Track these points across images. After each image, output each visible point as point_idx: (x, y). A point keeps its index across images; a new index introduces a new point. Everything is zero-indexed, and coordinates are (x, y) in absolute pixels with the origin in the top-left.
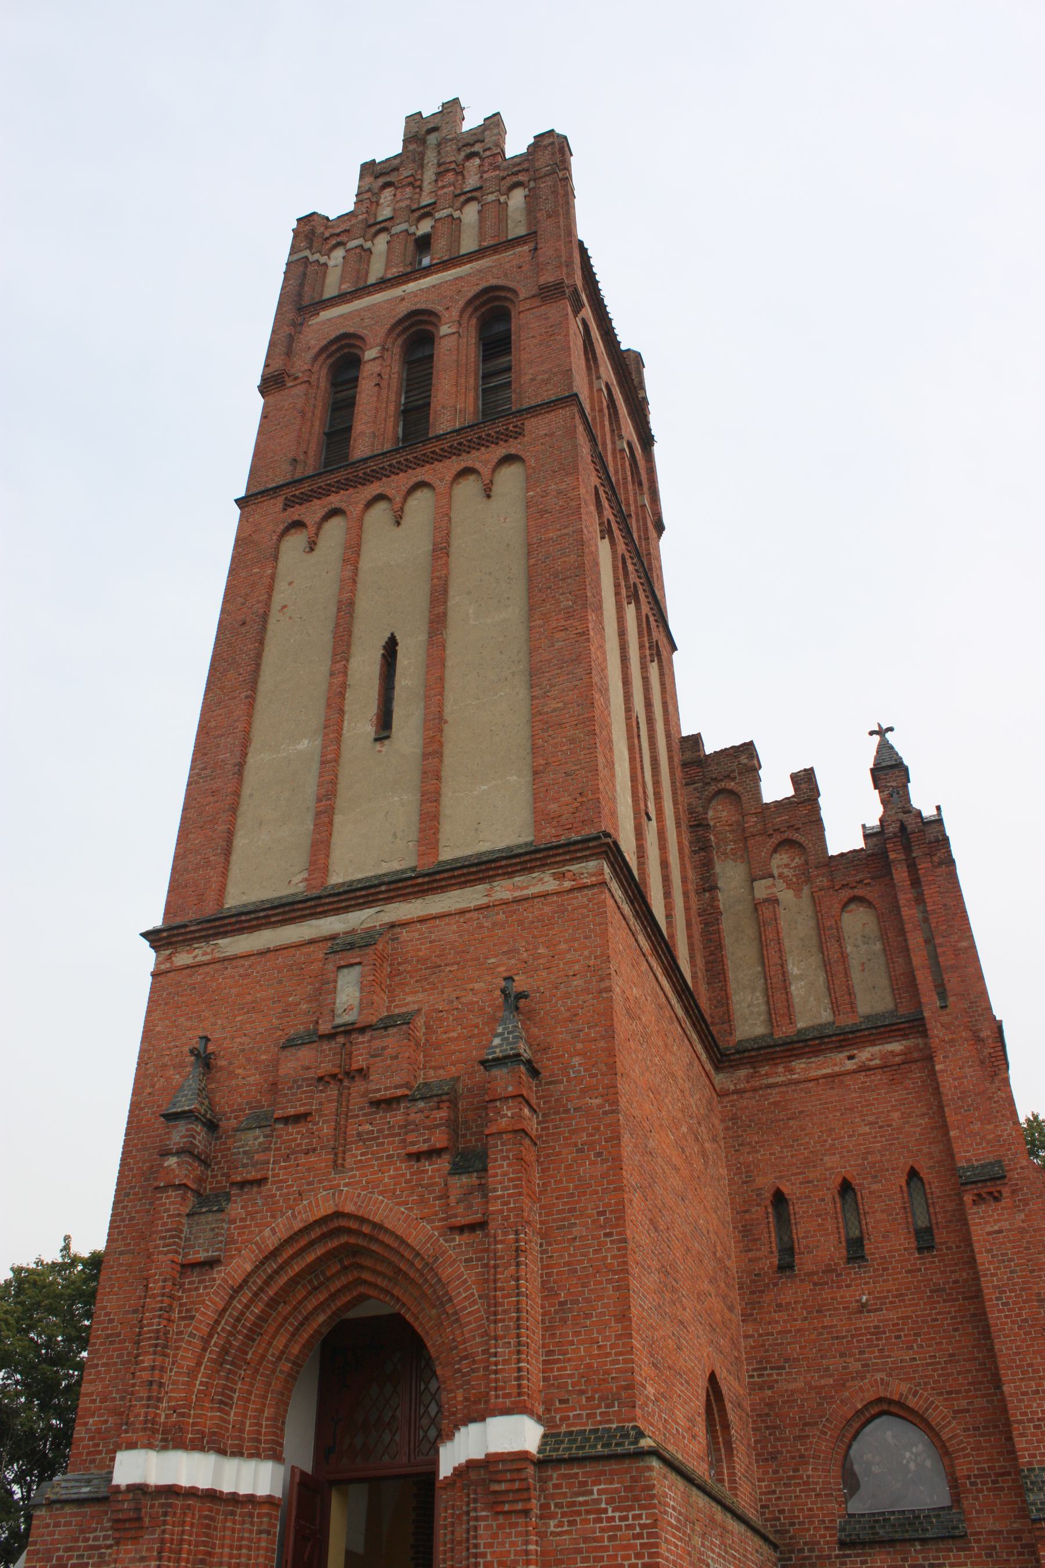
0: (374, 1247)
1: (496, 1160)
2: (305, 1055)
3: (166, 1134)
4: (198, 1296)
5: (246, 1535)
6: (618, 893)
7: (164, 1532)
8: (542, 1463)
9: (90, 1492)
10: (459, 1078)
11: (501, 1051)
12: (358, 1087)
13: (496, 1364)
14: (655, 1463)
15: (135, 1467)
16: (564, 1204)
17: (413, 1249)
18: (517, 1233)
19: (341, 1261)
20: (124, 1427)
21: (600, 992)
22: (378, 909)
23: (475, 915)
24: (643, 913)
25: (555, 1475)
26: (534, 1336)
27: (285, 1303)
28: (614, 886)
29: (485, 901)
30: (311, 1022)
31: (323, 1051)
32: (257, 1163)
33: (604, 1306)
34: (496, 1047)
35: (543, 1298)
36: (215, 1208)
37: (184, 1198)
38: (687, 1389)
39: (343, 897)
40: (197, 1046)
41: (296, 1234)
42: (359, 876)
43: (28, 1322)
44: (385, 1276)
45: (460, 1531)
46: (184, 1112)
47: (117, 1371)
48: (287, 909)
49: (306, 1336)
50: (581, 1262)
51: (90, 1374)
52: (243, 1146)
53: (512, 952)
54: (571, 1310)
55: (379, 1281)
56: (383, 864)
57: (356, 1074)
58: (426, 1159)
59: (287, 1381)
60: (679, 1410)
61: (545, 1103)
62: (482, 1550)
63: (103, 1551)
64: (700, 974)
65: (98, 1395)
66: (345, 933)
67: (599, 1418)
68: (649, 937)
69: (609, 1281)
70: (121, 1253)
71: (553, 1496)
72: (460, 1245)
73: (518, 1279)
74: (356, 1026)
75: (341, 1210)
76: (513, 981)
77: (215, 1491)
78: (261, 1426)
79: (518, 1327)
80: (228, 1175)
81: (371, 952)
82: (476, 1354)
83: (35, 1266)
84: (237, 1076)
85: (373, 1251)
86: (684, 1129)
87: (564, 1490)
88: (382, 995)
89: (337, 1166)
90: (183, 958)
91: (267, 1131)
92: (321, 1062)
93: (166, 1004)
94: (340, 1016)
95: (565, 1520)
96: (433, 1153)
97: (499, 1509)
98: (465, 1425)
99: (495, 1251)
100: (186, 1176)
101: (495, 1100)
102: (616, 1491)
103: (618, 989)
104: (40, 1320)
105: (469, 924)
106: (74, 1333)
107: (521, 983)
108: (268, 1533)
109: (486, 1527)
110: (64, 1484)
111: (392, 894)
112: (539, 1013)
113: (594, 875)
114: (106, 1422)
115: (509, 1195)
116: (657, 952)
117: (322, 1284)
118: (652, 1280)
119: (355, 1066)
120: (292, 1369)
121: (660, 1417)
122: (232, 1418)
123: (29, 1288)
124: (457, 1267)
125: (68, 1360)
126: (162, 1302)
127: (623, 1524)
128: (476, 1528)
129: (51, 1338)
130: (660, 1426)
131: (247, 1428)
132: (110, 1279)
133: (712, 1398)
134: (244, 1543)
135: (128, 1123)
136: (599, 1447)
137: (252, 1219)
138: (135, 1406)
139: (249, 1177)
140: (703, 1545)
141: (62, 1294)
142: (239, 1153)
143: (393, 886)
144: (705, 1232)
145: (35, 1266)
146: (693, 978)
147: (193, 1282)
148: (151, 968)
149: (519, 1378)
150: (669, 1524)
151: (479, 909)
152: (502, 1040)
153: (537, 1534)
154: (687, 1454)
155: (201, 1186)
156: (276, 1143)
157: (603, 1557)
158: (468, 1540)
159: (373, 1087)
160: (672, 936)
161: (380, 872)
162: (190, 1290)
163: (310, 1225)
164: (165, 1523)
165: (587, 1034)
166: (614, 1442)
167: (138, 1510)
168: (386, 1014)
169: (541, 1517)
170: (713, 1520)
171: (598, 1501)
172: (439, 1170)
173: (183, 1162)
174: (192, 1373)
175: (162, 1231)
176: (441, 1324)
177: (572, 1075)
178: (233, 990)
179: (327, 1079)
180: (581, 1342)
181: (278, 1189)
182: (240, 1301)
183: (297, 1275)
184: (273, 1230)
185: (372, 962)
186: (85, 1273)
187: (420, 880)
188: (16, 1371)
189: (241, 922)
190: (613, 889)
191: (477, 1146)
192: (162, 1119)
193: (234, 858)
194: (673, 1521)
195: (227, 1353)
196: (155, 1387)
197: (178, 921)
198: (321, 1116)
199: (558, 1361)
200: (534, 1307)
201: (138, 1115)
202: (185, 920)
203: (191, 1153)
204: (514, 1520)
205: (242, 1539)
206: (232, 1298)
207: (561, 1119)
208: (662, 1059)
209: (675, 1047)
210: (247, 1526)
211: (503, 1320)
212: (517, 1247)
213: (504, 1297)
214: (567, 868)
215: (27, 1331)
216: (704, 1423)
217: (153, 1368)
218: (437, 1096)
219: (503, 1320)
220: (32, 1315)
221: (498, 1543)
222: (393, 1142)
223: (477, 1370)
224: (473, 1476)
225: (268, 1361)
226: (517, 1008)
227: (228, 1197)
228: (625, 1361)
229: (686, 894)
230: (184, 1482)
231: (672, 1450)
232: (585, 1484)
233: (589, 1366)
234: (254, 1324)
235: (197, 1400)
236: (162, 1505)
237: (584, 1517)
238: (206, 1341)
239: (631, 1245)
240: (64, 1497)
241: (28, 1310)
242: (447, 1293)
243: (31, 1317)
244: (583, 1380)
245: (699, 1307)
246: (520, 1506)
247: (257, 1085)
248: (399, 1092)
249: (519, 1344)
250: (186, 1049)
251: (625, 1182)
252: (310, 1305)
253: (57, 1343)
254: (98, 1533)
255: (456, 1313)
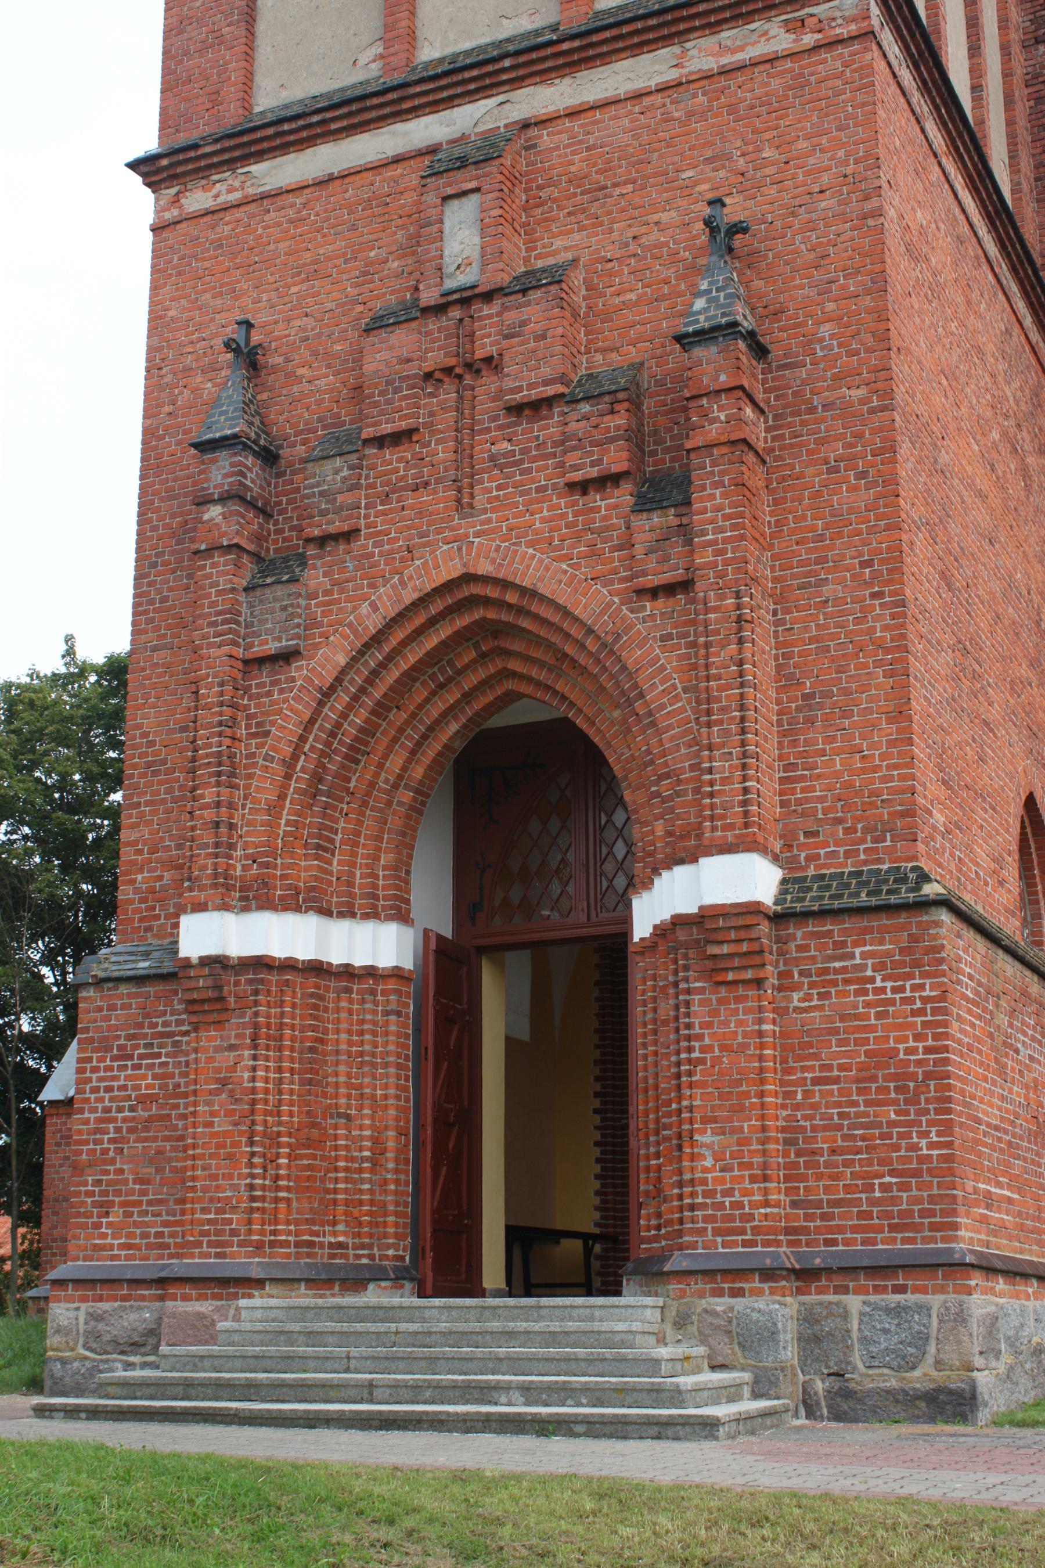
0: (525, 623)
1: (703, 488)
2: (402, 340)
3: (201, 473)
4: (272, 703)
5: (369, 1017)
6: (894, 51)
7: (256, 1014)
8: (779, 918)
9: (150, 967)
10: (642, 364)
11: (707, 319)
12: (487, 385)
13: (711, 783)
14: (945, 916)
15: (206, 934)
16: (809, 551)
17: (583, 624)
18: (738, 595)
19: (476, 645)
20: (186, 884)
21: (865, 218)
22: (501, 98)
23: (658, 99)
24: (934, 83)
25: (799, 934)
26: (767, 744)
27: (398, 708)
28: (887, 37)
29: (673, 75)
30: (407, 289)
31: (428, 334)
32: (341, 508)
33: (871, 699)
34: (699, 313)
35: (779, 690)
36: (285, 578)
37: (237, 565)
38: (992, 818)
39: (444, 82)
40: (235, 336)
41: (407, 609)
42: (467, 45)
43: (31, 757)
44: (542, 664)
45: (666, 1009)
46: (225, 438)
47: (168, 811)
48: (354, 107)
49: (432, 754)
50: (835, 637)
51: (130, 816)
52: (318, 485)
53: (719, 159)
54: (821, 706)
55: (534, 673)
56: (505, 21)
57: (483, 366)
58: (597, 491)
59: (408, 817)
60: (981, 846)
61: (777, 398)
62: (697, 1030)
63: (177, 1038)
64: (1025, 186)
65: (144, 845)
66: (451, 142)
67: (862, 857)
68: (944, 124)
69: (878, 664)
70: (154, 649)
71: (797, 961)
72: (652, 616)
73: (741, 663)
74: (477, 291)
75: (472, 571)
76: (724, 205)
77: (321, 962)
78: (377, 877)
79: (743, 731)
80: (300, 529)
81: (494, 169)
82: (682, 770)
83: (28, 680)
84: (299, 380)
85: (524, 630)
86: (995, 435)
87: (813, 953)
88: (515, 238)
89: (462, 506)
90: (197, 200)
91: (353, 459)
92: (427, 351)
93: (179, 274)
94: (451, 276)
95: (815, 992)
96: (607, 481)
97: (720, 978)
98: (669, 868)
99: (706, 623)
100: (238, 532)
101: (701, 396)
102: (888, 954)
103: (892, 213)
104: (46, 753)
105: (649, 115)
106: (95, 769)
107: (735, 210)
108: (398, 1014)
109: (702, 1003)
110: (113, 959)
111: (521, 72)
112: (766, 257)
113: (853, 20)
114: (160, 878)
115: (725, 541)
116: (957, 149)
117: (450, 680)
118: (944, 661)
119: (480, 354)
120: (414, 799)
121: (952, 855)
122: (335, 867)
123: (25, 710)
124: (650, 649)
125: (92, 805)
126: (221, 714)
127: (898, 996)
128: (688, 1004)
129: (65, 776)
130: (953, 868)
131: (358, 881)
132: (143, 686)
133: (1029, 830)
134: (366, 1027)
135: (143, 460)
136: (863, 895)
137: (341, 591)
138: (199, 855)
139: (332, 529)
140: (1011, 1025)
141: (72, 717)
142: (313, 495)
143: (522, 59)
144: (1025, 592)
145: (28, 680)
146: (1013, 192)
147: (264, 685)
148: (148, 217)
149: (745, 803)
150: (964, 997)
151: (662, 89)
152: (708, 301)
153: (774, 1011)
154: (991, 905)
155: (261, 547)
156: (367, 477)
157: (868, 1039)
158: (677, 1018)
159: (509, 383)
160: (981, 122)
161: (501, 37)
162: (259, 696)
163: (428, 595)
164: (256, 1003)
165: (843, 288)
166: (885, 888)
167: (218, 987)
168: (523, 269)
169: (780, 989)
170: (1025, 993)
171: (863, 967)
172: (616, 506)
173: (232, 513)
174: (274, 809)
175: (210, 614)
176: (629, 730)
177: (820, 353)
178: (281, 245)
179: (437, 375)
180: (838, 752)
181: (376, 545)
182: (332, 709)
183: (413, 668)
184: (374, 607)
185: (497, 186)
186: (101, 685)
187: (565, 46)
188: (22, 822)
189: (284, 133)
190: (885, 44)
191: (673, 468)
192: (193, 451)
193: (261, 27)
194: (969, 993)
195: (321, 780)
196: (223, 830)
197: (183, 139)
198: (432, 433)
199: (803, 778)
200: (765, 701)
201: (156, 448)
202: (194, 136)
203: (242, 499)
204: (741, 993)
205: (363, 1022)
206: (321, 704)
207: (803, 423)
208: (962, 324)
209: (983, 306)
210: (368, 1006)
211: (720, 722)
212: (739, 616)
213: (721, 689)
214: (807, 10)
215: (30, 769)
216: (1016, 865)
217: (218, 805)
218: (609, 393)
219: (720, 722)
220: (34, 747)
221: (720, 1023)
222: (546, 467)
223: (684, 793)
224: (682, 935)
225: (380, 790)
226: (730, 250)
227: (303, 561)
228: (902, 778)
229: (1005, 49)
230: (279, 952)
231: (969, 899)
232: (843, 944)
233: (849, 785)
234: (356, 739)
235: (284, 846)
236: (250, 982)
237: (840, 988)
238: (290, 765)
239: (912, 610)
240: (116, 974)
241: (28, 740)
242: (636, 686)
243: (33, 750)
244: (839, 804)
245: (1012, 701)
246: (749, 975)
247: (332, 391)
248: (551, 390)
249: (745, 755)
250: (218, 342)
251: (904, 515)
252: (435, 710)
253: (74, 784)
254: (168, 1018)
255: (650, 714)
